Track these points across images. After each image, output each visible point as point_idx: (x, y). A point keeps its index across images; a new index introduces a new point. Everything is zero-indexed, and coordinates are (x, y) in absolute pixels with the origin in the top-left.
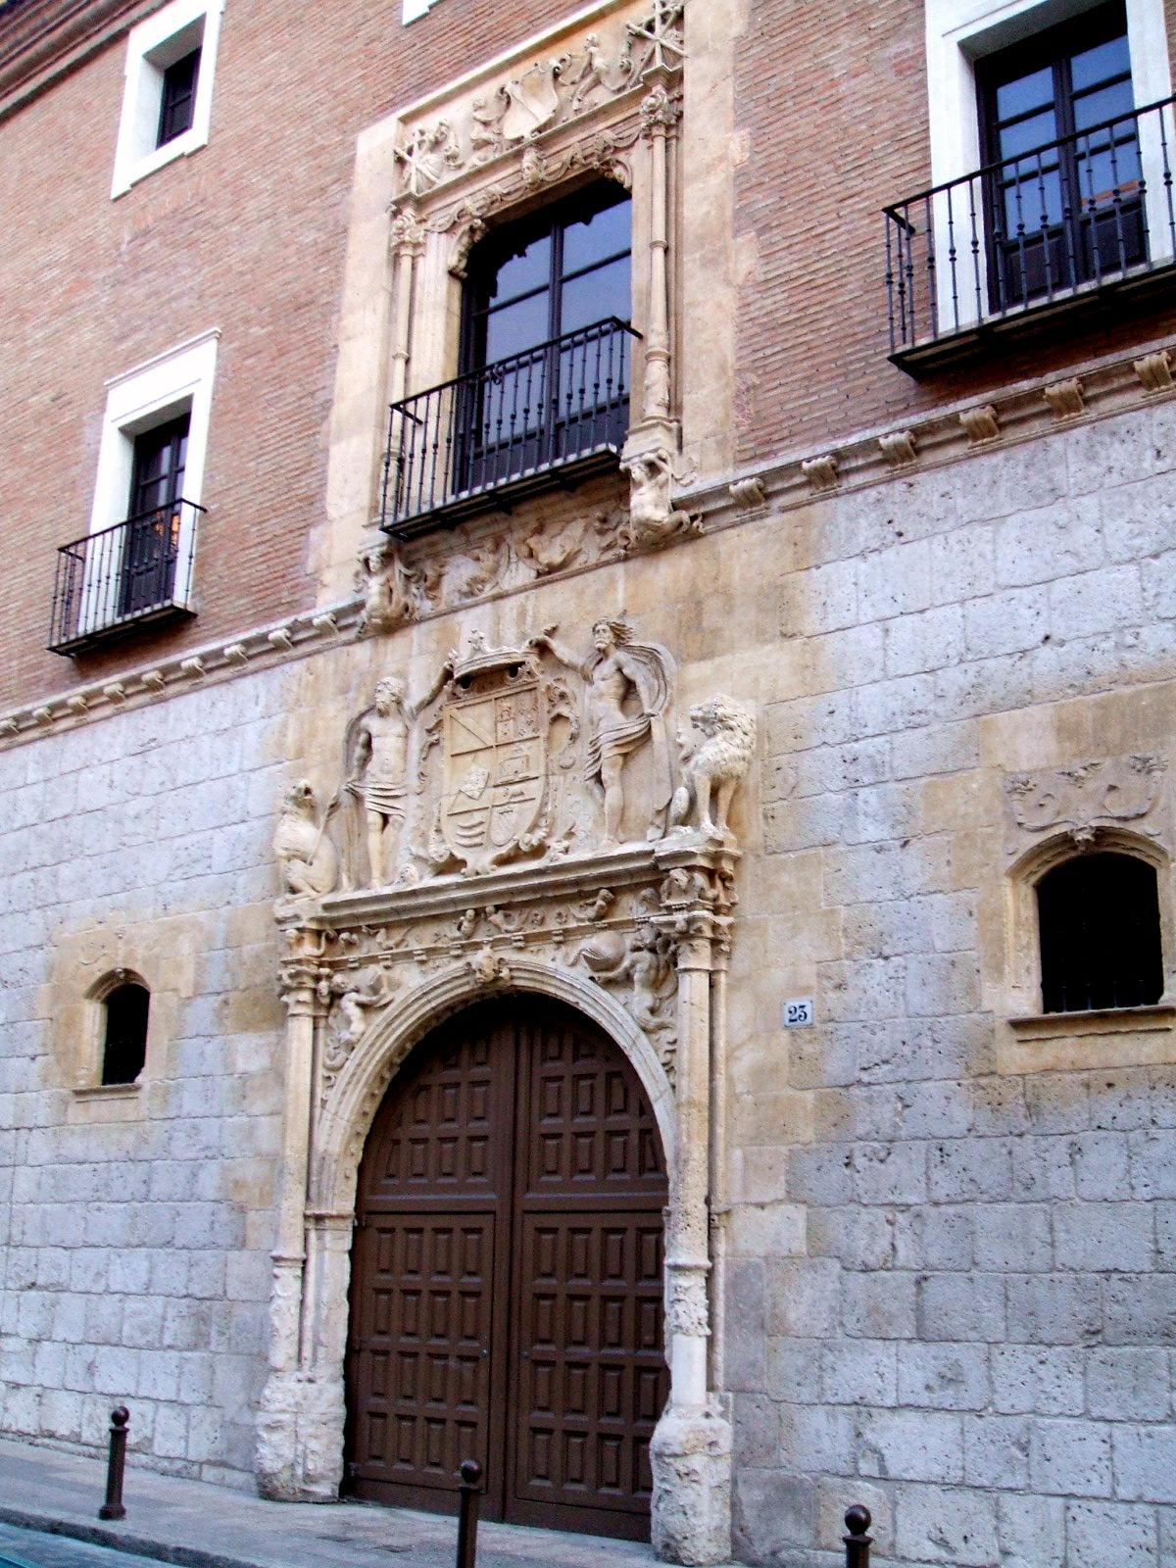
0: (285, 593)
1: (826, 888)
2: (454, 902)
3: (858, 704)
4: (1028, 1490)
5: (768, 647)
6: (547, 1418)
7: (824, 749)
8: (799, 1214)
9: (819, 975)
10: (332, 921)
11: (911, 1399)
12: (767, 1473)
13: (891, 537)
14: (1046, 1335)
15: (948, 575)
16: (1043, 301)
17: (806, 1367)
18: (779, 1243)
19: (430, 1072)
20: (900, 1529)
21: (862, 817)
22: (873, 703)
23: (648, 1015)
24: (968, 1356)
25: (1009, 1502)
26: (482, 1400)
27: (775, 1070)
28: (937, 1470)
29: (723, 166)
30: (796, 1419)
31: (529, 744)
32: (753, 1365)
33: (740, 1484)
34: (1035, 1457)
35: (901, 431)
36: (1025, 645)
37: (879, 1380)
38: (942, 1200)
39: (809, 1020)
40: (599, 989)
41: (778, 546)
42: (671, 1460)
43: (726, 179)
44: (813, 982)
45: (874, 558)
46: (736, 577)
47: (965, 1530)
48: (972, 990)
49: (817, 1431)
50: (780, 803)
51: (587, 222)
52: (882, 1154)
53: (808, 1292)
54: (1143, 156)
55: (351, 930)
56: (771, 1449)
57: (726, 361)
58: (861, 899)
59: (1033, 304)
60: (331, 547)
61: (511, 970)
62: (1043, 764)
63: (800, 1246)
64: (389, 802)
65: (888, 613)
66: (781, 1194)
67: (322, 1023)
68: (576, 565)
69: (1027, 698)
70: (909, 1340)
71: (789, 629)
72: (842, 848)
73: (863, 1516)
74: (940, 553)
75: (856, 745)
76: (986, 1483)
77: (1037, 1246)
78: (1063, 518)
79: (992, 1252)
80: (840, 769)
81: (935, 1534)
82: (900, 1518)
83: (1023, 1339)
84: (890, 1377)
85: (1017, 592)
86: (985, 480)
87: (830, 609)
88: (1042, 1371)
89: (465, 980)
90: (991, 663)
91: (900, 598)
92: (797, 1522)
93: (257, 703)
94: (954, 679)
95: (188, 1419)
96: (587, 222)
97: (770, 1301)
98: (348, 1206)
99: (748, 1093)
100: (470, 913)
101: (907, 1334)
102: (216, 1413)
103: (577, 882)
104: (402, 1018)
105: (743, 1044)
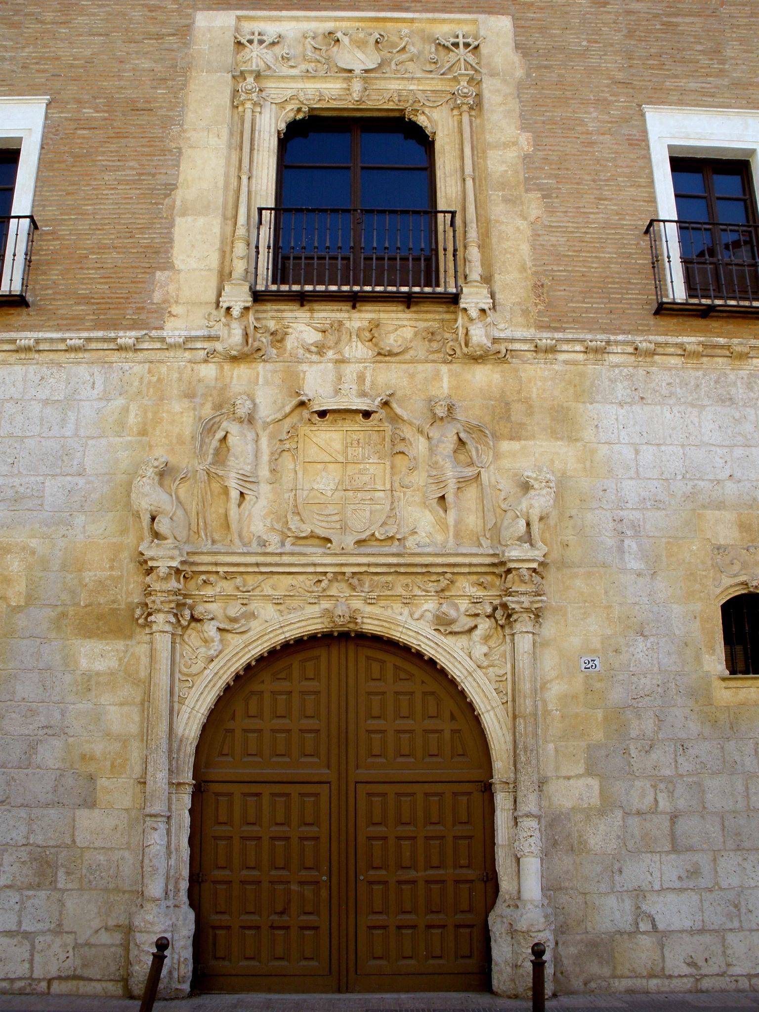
0: (130, 312)
1: (606, 592)
3: (622, 489)
4: (741, 929)
5: (559, 443)
6: (381, 919)
8: (595, 783)
11: (671, 885)
12: (578, 937)
14: (746, 844)
15: (673, 429)
16: (747, 303)
18: (582, 799)
20: (667, 959)
21: (627, 555)
22: (631, 489)
23: (483, 658)
24: (703, 860)
25: (730, 937)
27: (575, 697)
28: (687, 924)
29: (514, 148)
30: (597, 903)
32: (567, 872)
33: (560, 945)
34: (743, 910)
35: (650, 342)
36: (719, 477)
37: (649, 876)
38: (685, 773)
40: (443, 638)
41: (563, 384)
42: (535, 934)
43: (518, 157)
44: (599, 646)
45: (626, 407)
46: (534, 395)
47: (706, 955)
48: (698, 659)
49: (612, 908)
51: (406, 138)
52: (647, 748)
53: (602, 828)
56: (580, 922)
57: (525, 264)
58: (629, 601)
59: (742, 303)
60: (179, 289)
61: (363, 617)
62: (732, 542)
63: (596, 801)
64: (248, 485)
65: (638, 441)
66: (581, 771)
68: (407, 357)
69: (720, 506)
70: (668, 852)
74: (668, 415)
76: (717, 928)
77: (739, 799)
78: (737, 415)
79: (714, 800)
80: (611, 525)
81: (689, 960)
82: (667, 954)
83: (733, 847)
84: (657, 874)
85: (713, 448)
86: (692, 383)
87: (600, 430)
88: (745, 865)
90: (701, 484)
91: (645, 434)
92: (600, 963)
93: (93, 388)
94: (680, 487)
95: (33, 946)
96: (406, 138)
97: (576, 834)
100: (330, 576)
101: (666, 849)
102: (69, 939)
104: (259, 642)
105: (552, 680)
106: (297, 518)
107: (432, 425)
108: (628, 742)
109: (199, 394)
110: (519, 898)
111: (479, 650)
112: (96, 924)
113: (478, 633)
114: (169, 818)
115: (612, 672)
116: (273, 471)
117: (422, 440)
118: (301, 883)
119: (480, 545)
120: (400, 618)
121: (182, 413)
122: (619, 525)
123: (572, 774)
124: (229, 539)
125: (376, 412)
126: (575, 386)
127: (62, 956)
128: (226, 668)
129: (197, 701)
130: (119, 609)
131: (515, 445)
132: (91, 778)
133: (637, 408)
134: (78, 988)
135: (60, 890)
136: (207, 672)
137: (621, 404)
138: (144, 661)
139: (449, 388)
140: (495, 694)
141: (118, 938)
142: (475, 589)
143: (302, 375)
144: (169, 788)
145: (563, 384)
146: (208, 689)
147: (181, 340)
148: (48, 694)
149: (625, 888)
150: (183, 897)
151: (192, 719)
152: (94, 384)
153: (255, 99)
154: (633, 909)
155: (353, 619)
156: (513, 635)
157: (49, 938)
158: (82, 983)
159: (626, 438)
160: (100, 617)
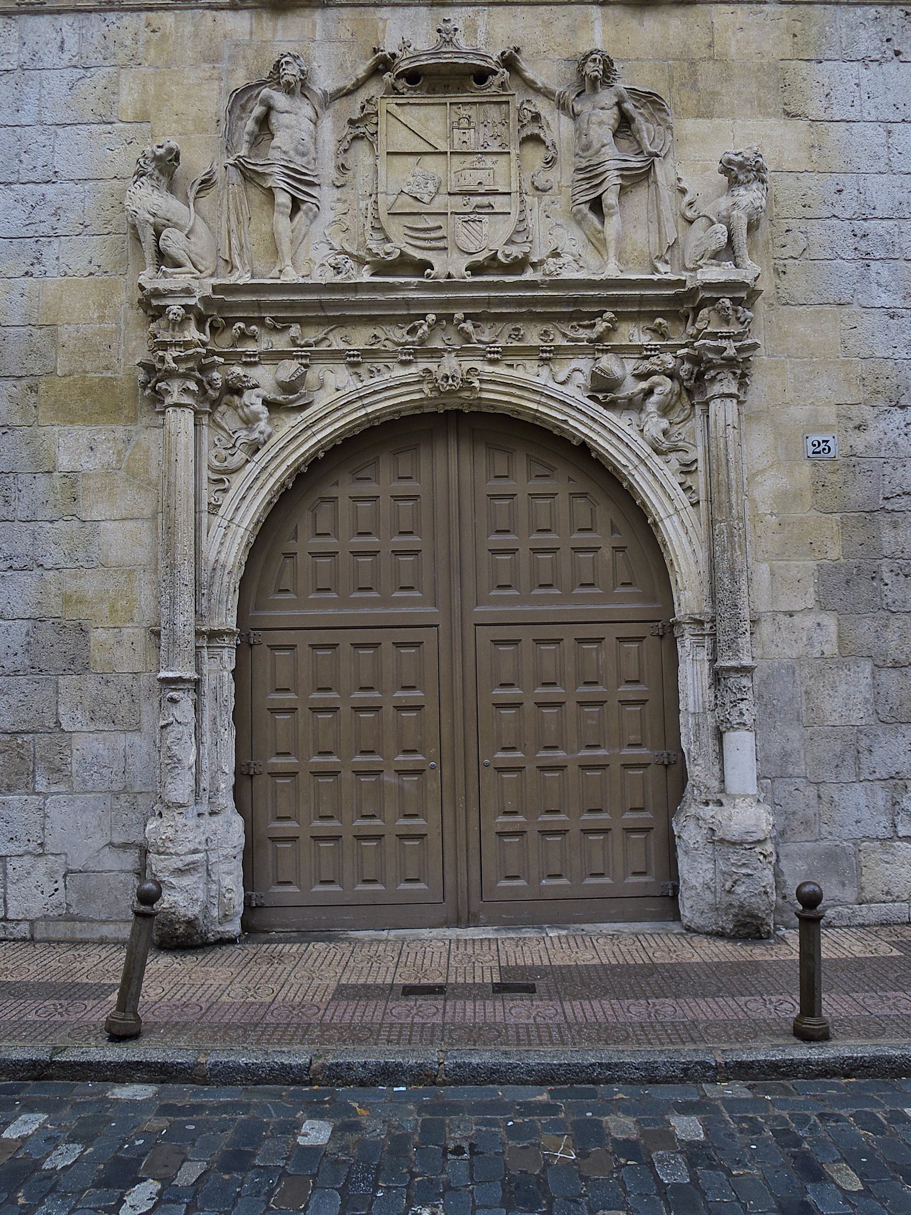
2: (408, 303)
5: (772, 121)
7: (835, 221)
8: (830, 622)
9: (838, 416)
10: (223, 306)
13: (890, 53)
17: (842, 753)
19: (337, 484)
26: (435, 816)
31: (495, 158)
39: (832, 454)
40: (601, 409)
46: (733, 50)
50: (790, 261)
54: (230, 14)
55: (248, 321)
58: (878, 355)
67: (205, 420)
71: (791, 108)
72: (856, 308)
73: (817, 889)
75: (866, 224)
89: (416, 387)
91: (900, 106)
98: (231, 622)
99: (772, 514)
100: (431, 317)
103: (575, 301)
106: (378, 236)
107: (578, 95)
108: (878, 562)
109: (226, 56)
110: (723, 791)
111: (655, 424)
112: (98, 841)
113: (651, 405)
114: (197, 683)
115: (853, 458)
116: (342, 168)
117: (566, 121)
118: (400, 773)
119: (656, 270)
120: (537, 380)
121: (200, 85)
122: (862, 242)
123: (797, 608)
124: (277, 269)
125: (495, 73)
126: (795, 36)
127: (49, 890)
128: (278, 460)
129: (237, 509)
130: (115, 379)
131: (702, 126)
132: (82, 630)
133: (891, 67)
134: (73, 932)
135: (38, 794)
136: (249, 466)
137: (865, 61)
138: (156, 454)
139: (604, 41)
140: (679, 489)
141: (130, 859)
142: (648, 337)
143: (381, 25)
144: (197, 640)
145: (777, 33)
146: (253, 492)
147: (179, 319)
148: (11, 508)
149: (878, 775)
150: (226, 800)
151: (229, 536)
152: (62, 42)
153: (273, 1021)
154: (889, 805)
155: (467, 385)
156: (707, 403)
157: (27, 860)
158: (78, 925)
159: (873, 112)
160: (87, 391)
